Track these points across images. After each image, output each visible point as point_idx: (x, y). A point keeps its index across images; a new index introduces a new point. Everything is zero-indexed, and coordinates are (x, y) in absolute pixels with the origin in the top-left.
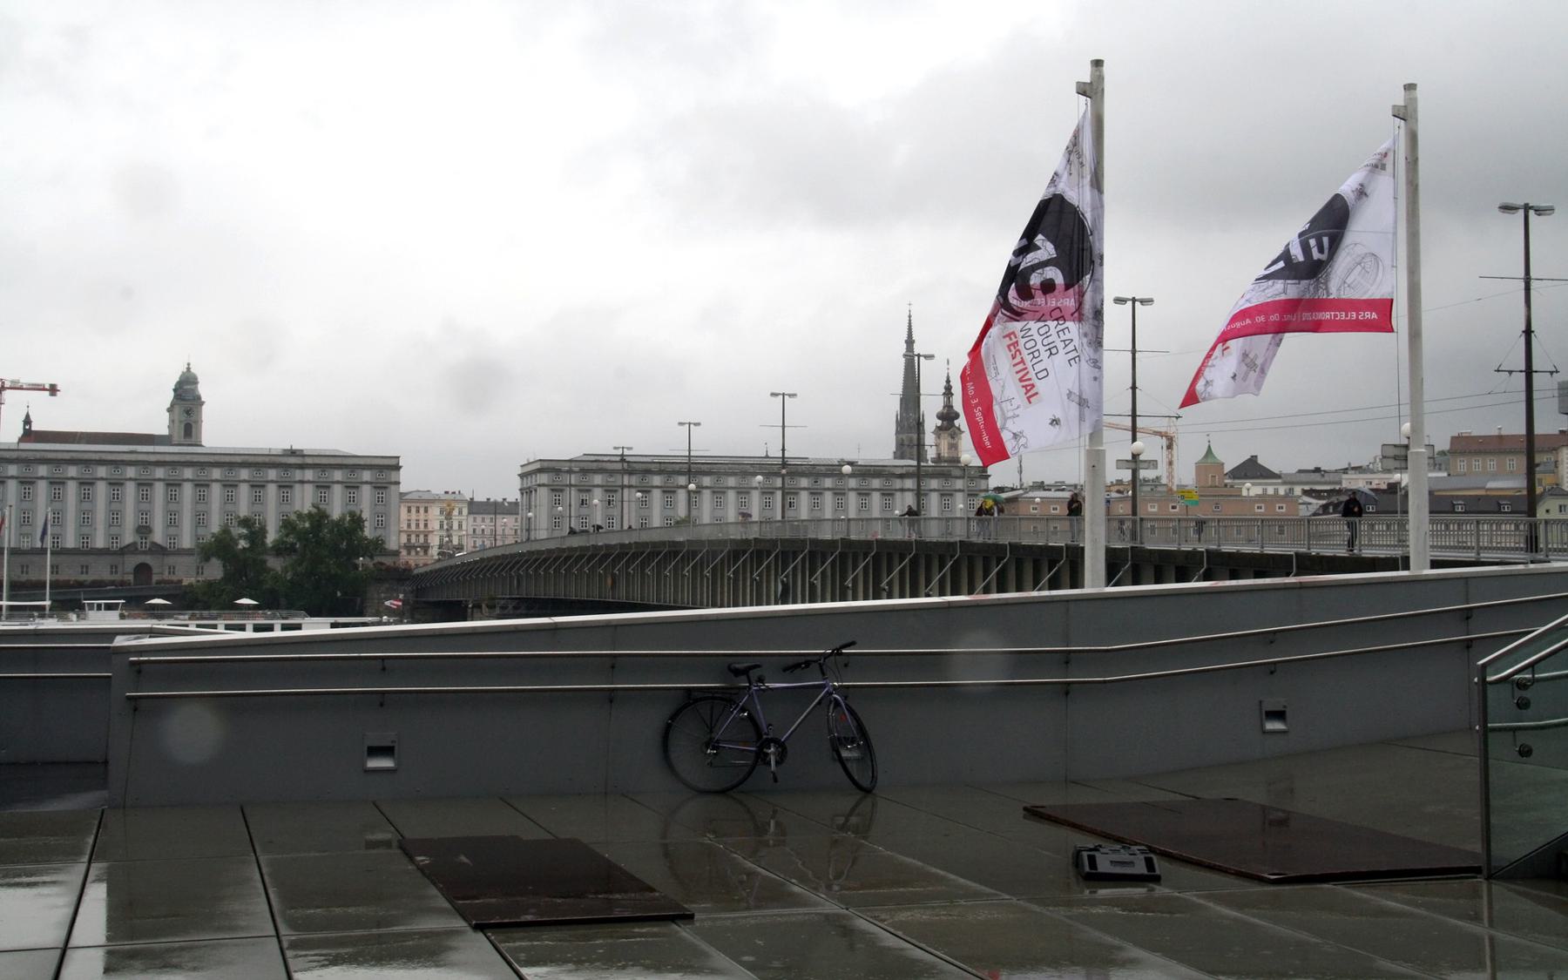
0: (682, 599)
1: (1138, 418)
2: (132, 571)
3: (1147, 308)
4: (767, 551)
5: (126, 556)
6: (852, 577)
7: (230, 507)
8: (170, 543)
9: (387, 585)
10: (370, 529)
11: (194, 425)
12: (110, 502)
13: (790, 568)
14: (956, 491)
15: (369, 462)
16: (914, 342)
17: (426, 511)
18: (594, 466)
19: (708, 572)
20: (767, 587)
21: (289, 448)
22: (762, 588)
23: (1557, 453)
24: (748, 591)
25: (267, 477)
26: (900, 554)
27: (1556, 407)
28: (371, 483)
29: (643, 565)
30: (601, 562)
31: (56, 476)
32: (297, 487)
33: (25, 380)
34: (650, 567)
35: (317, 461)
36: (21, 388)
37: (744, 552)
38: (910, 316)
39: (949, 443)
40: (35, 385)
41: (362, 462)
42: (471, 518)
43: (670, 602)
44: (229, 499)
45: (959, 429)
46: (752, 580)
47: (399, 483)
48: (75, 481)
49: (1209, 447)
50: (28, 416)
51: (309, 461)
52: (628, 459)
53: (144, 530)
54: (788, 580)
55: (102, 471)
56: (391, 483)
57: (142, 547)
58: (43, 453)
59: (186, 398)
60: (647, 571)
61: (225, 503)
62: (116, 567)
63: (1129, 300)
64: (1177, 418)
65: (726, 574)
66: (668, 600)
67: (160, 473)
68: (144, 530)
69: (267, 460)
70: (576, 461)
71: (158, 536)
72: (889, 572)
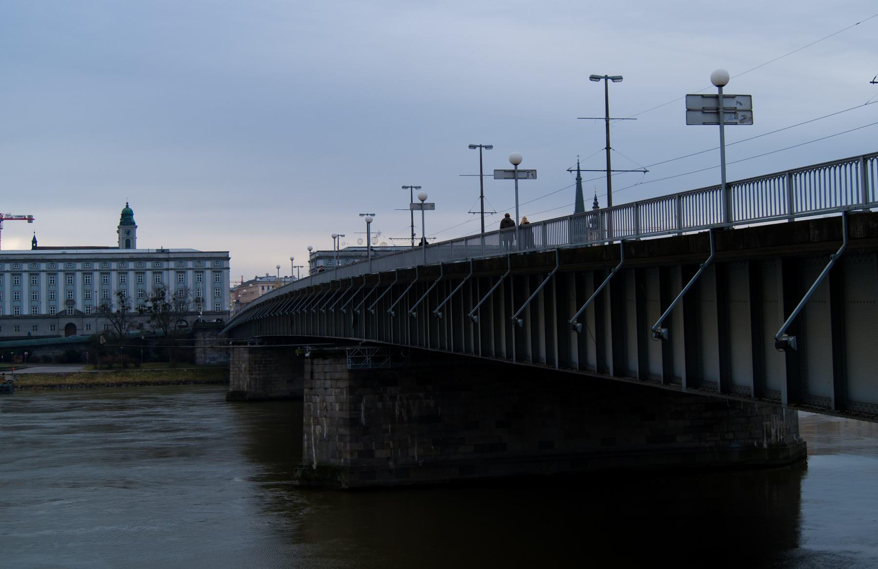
1: (485, 214)
2: (64, 328)
3: (489, 151)
5: (60, 319)
7: (140, 287)
8: (87, 310)
9: (210, 333)
11: (131, 240)
12: (49, 285)
14: (188, 269)
15: (209, 255)
16: (581, 179)
18: (353, 254)
21: (161, 248)
25: (128, 267)
28: (211, 269)
31: (15, 270)
32: (165, 272)
33: (14, 214)
35: (177, 256)
36: (11, 219)
38: (578, 163)
40: (20, 216)
41: (205, 255)
43: (391, 342)
44: (140, 282)
47: (229, 268)
48: (27, 273)
49: (34, 236)
50: (34, 238)
51: (172, 256)
52: (374, 249)
53: (70, 302)
54: (524, 323)
55: (43, 266)
56: (224, 269)
57: (69, 313)
58: (35, 256)
61: (14, 286)
62: (54, 326)
64: (645, 172)
67: (79, 266)
68: (70, 302)
69: (145, 256)
70: (345, 251)
71: (79, 306)
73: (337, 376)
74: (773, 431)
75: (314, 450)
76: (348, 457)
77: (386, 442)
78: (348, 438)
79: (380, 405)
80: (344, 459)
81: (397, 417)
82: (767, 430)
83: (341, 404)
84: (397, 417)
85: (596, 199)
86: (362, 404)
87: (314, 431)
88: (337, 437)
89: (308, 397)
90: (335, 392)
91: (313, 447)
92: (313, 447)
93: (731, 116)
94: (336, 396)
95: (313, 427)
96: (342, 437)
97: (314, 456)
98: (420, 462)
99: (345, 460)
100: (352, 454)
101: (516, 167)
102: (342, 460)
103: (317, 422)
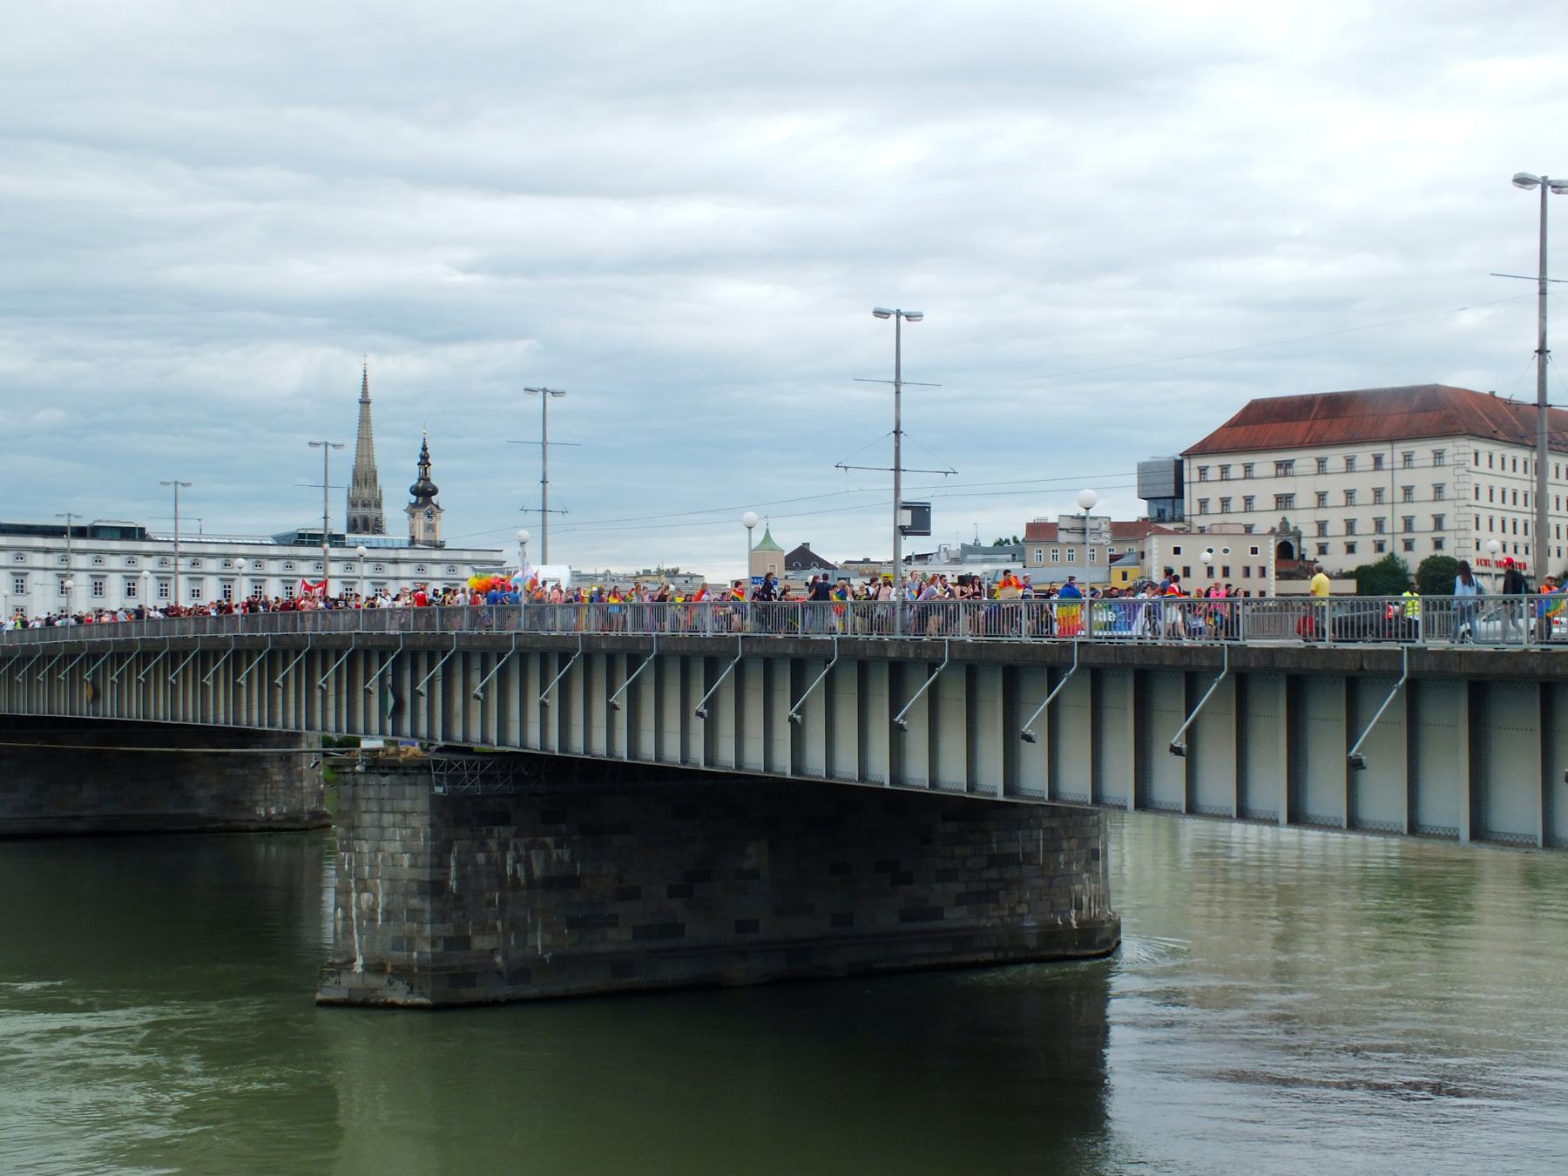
0: (38, 708)
3: (558, 399)
4: (184, 652)
6: (246, 672)
7: (20, 601)
13: (211, 672)
19: (88, 676)
20: (155, 692)
22: (149, 689)
23: (1143, 543)
24: (255, 703)
26: (498, 654)
27: (1136, 494)
34: (21, 673)
39: (425, 524)
43: (5, 712)
45: (437, 506)
46: (139, 681)
60: (85, 677)
63: (893, 313)
65: (109, 679)
66: (191, 716)
72: (285, 666)
73: (407, 805)
74: (1085, 899)
75: (356, 936)
76: (428, 949)
77: (490, 922)
78: (428, 916)
79: (481, 858)
80: (419, 953)
81: (509, 880)
82: (1076, 899)
84: (509, 880)
85: (424, 449)
86: (452, 856)
88: (405, 913)
89: (345, 842)
90: (401, 836)
91: (355, 931)
92: (355, 931)
94: (403, 839)
95: (354, 895)
96: (414, 914)
97: (357, 946)
98: (546, 956)
99: (420, 953)
100: (434, 944)
101: (1087, 513)
102: (415, 955)
103: (363, 887)
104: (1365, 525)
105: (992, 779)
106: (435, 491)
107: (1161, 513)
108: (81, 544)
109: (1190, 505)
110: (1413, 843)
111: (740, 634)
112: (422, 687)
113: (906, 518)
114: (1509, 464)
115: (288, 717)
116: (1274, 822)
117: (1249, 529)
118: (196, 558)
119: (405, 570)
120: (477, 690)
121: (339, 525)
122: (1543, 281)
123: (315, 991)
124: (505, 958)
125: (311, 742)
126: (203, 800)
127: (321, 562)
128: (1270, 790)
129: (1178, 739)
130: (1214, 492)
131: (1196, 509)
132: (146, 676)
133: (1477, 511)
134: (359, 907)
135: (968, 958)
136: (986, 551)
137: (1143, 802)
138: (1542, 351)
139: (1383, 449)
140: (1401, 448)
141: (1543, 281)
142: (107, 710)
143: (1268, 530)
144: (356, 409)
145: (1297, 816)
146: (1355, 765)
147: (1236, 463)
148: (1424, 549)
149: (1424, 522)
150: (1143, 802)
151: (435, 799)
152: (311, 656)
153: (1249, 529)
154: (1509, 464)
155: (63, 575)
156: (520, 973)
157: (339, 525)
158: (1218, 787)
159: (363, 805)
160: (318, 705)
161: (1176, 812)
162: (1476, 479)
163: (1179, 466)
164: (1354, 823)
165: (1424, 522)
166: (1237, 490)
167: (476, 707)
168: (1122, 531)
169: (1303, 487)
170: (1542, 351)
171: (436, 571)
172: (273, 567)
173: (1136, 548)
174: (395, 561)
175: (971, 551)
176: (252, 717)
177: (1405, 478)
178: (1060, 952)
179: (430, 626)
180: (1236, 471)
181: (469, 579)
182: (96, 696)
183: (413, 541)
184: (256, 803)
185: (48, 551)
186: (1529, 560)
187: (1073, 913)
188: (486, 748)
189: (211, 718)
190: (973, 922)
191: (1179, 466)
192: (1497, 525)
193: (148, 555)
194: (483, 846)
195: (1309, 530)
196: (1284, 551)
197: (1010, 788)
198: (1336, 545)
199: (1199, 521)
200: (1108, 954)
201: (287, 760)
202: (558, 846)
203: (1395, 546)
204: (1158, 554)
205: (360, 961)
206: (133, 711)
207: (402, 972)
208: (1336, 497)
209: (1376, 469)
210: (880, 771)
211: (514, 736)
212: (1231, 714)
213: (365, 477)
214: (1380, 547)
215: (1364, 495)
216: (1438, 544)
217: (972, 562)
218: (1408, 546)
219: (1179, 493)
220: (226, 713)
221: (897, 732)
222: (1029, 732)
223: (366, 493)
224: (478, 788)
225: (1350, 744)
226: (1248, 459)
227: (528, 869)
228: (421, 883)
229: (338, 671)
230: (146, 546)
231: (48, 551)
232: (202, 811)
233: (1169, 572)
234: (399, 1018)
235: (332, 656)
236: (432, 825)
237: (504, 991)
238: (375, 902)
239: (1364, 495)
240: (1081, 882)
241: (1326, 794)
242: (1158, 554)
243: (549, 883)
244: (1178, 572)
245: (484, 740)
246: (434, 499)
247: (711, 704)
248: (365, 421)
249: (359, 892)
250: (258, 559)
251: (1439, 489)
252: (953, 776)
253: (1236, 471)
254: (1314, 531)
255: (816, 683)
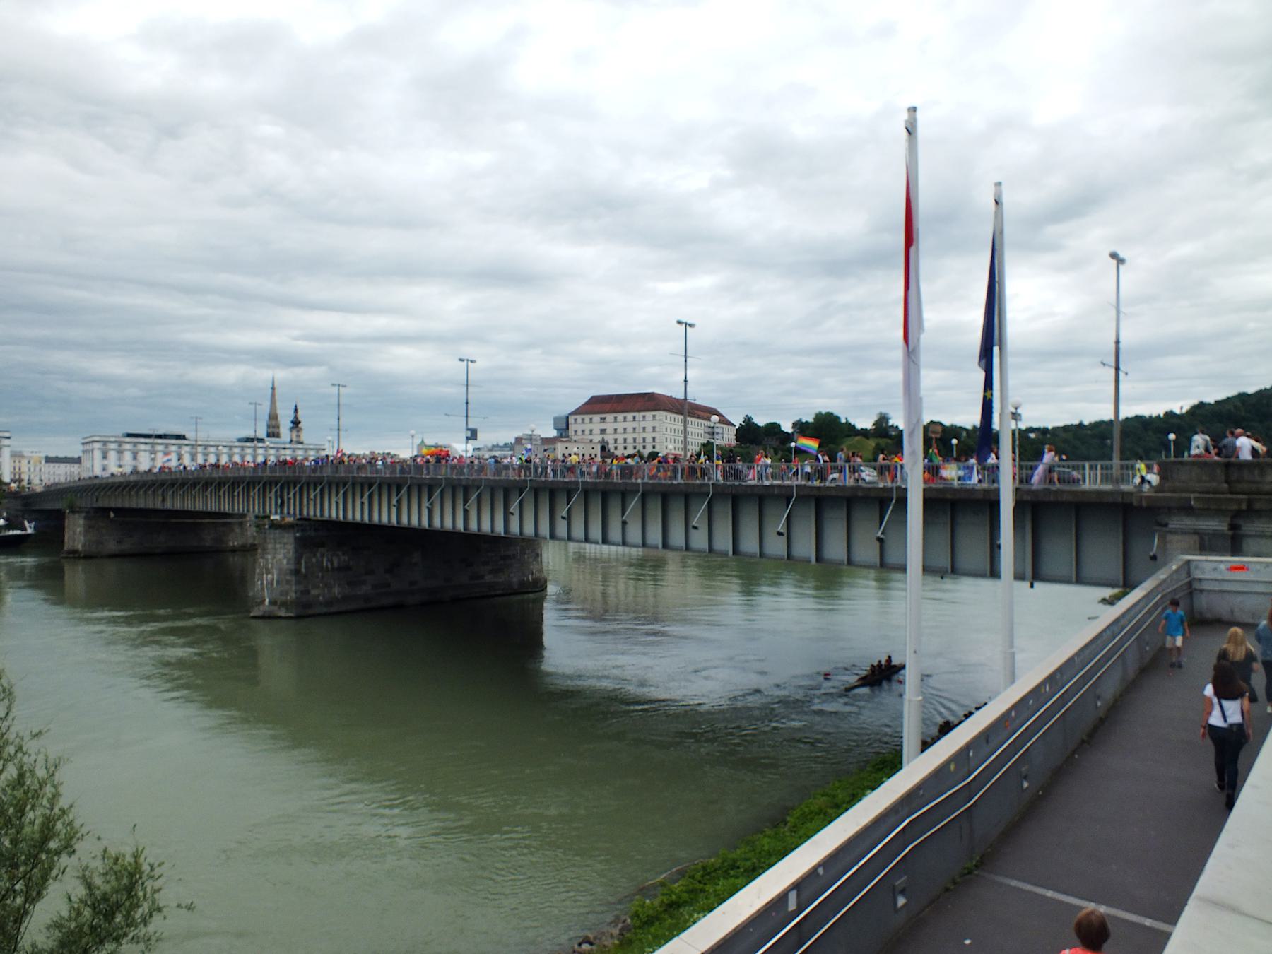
3: (344, 388)
10: (819, 488)
17: (20, 462)
29: (130, 490)
30: (97, 490)
37: (187, 484)
42: (47, 465)
59: (1032, 586)
73: (285, 541)
74: (534, 572)
78: (294, 582)
79: (314, 560)
83: (289, 560)
85: (296, 406)
87: (267, 577)
93: (66, 467)
94: (284, 554)
95: (265, 576)
96: (288, 582)
100: (296, 593)
103: (268, 572)
104: (630, 440)
105: (500, 528)
106: (300, 422)
107: (561, 434)
108: (160, 441)
109: (571, 432)
110: (646, 550)
111: (409, 476)
112: (291, 495)
113: (469, 434)
114: (673, 419)
115: (239, 507)
116: (597, 543)
117: (591, 441)
118: (206, 447)
119: (288, 452)
120: (312, 497)
121: (262, 433)
122: (686, 357)
123: (250, 612)
124: (324, 597)
125: (251, 517)
126: (208, 540)
127: (255, 448)
128: (596, 532)
129: (564, 514)
130: (579, 427)
131: (573, 433)
132: (184, 492)
133: (666, 436)
134: (267, 580)
135: (493, 593)
136: (501, 447)
137: (553, 536)
138: (686, 381)
139: (636, 414)
140: (642, 414)
141: (686, 357)
142: (168, 505)
143: (597, 441)
144: (270, 391)
145: (605, 541)
146: (624, 523)
147: (587, 418)
148: (649, 450)
149: (649, 440)
150: (553, 536)
151: (296, 538)
152: (248, 484)
153: (591, 441)
154: (673, 419)
155: (153, 452)
156: (329, 603)
157: (262, 433)
158: (578, 531)
159: (268, 541)
160: (268, 504)
161: (563, 540)
162: (666, 425)
163: (567, 418)
164: (624, 543)
165: (649, 440)
166: (587, 427)
167: (312, 503)
168: (546, 441)
169: (609, 427)
170: (686, 381)
171: (300, 452)
172: (237, 450)
173: (553, 447)
174: (285, 449)
175: (495, 447)
176: (226, 507)
177: (643, 424)
178: (526, 590)
179: (295, 472)
180: (587, 420)
181: (312, 455)
182: (163, 500)
183: (291, 441)
184: (230, 541)
185: (146, 444)
186: (682, 453)
187: (530, 576)
188: (315, 518)
189: (209, 508)
190: (495, 580)
191: (567, 418)
192: (673, 441)
193: (187, 445)
194: (315, 556)
195: (611, 442)
196: (603, 449)
197: (506, 532)
198: (621, 447)
199: (574, 438)
200: (542, 590)
201: (241, 524)
202: (344, 554)
203: (640, 448)
204: (560, 449)
205: (267, 601)
206: (178, 505)
207: (284, 604)
208: (620, 430)
209: (653, 420)
210: (425, 523)
211: (326, 514)
212: (728, 513)
213: (273, 417)
214: (635, 448)
215: (630, 430)
216: (654, 447)
217: (496, 451)
218: (644, 447)
219: (568, 428)
220: (243, 508)
221: (466, 512)
222: (696, 525)
223: (274, 423)
224: (313, 534)
225: (623, 515)
226: (591, 416)
227: (332, 564)
228: (291, 570)
229: (259, 490)
230: (186, 442)
231: (146, 444)
232: (207, 544)
233: (563, 455)
234: (283, 622)
235: (257, 484)
236: (295, 548)
237: (325, 610)
238: (273, 579)
239: (630, 430)
240: (533, 565)
241: (615, 534)
242: (560, 449)
243: (340, 569)
244: (567, 455)
245: (315, 515)
246: (300, 425)
247: (399, 502)
248: (273, 395)
249: (267, 574)
250: (231, 448)
251: (654, 428)
252: (486, 527)
253: (587, 420)
254: (613, 442)
255: (437, 494)
